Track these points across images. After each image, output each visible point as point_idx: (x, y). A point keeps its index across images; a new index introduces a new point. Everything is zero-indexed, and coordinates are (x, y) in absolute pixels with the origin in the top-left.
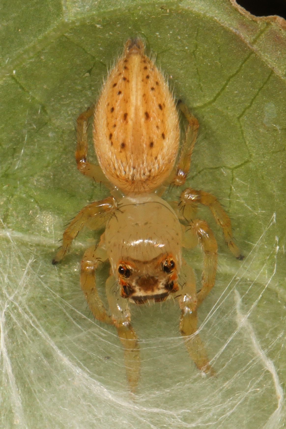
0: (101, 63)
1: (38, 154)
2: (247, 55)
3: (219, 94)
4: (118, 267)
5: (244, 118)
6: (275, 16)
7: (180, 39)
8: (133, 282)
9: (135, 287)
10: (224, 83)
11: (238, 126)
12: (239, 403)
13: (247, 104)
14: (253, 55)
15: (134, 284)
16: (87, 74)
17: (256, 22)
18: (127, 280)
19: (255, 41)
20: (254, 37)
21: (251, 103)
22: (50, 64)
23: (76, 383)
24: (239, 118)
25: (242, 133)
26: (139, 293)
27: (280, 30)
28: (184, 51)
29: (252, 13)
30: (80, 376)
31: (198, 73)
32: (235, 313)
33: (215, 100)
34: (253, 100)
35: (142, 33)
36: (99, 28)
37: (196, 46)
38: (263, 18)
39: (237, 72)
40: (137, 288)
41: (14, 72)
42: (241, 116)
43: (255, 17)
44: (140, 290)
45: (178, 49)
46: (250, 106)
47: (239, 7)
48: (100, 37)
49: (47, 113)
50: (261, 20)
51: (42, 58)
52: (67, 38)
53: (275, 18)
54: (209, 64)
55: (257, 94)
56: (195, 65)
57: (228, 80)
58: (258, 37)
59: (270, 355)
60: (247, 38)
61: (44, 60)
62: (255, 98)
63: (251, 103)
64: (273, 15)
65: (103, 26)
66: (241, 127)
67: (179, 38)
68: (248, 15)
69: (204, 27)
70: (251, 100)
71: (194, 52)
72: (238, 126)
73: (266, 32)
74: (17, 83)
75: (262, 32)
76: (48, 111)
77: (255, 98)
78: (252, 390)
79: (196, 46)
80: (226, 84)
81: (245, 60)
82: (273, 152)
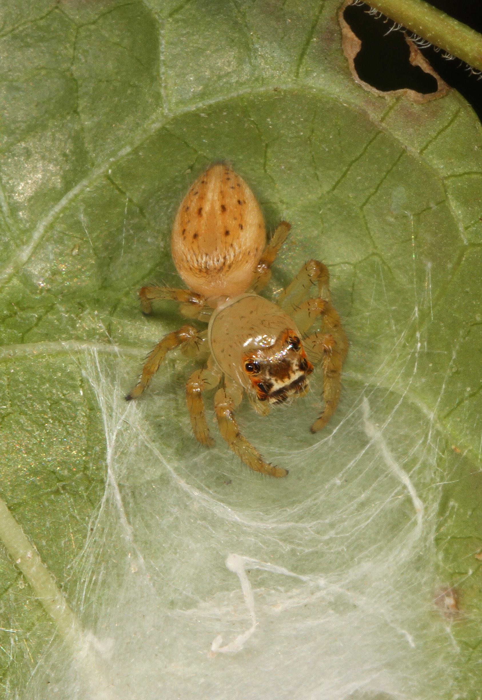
0: (204, 157)
1: (136, 263)
2: (374, 135)
3: (338, 182)
4: (245, 367)
5: (368, 206)
6: (405, 90)
7: (294, 125)
8: (266, 375)
9: (270, 379)
10: (344, 169)
11: (361, 216)
12: (375, 514)
13: (372, 190)
14: (381, 135)
15: (268, 377)
16: (189, 171)
17: (383, 98)
18: (259, 377)
19: (383, 119)
20: (382, 115)
21: (377, 189)
22: (149, 161)
23: (196, 506)
24: (361, 208)
25: (366, 223)
26: (277, 385)
27: (412, 104)
28: (300, 137)
29: (378, 88)
30: (200, 498)
31: (314, 161)
32: (363, 423)
33: (334, 188)
34: (379, 185)
35: (250, 120)
36: (203, 117)
37: (313, 131)
38: (392, 92)
39: (361, 155)
40: (273, 381)
41: (110, 171)
42: (364, 204)
43: (381, 92)
44: (276, 380)
45: (291, 135)
46: (376, 192)
47: (363, 84)
48: (203, 128)
49: (145, 217)
50: (389, 96)
51: (140, 154)
52: (167, 130)
53: (406, 92)
54: (327, 150)
55: (385, 178)
56: (311, 152)
57: (350, 165)
58: (387, 114)
59: (407, 467)
60: (374, 116)
61: (142, 157)
62: (382, 182)
63: (377, 189)
64: (403, 88)
65: (209, 115)
66: (364, 217)
67: (293, 123)
68: (375, 92)
69: (323, 109)
70: (376, 186)
71: (309, 138)
72: (361, 216)
73: (396, 108)
74: (113, 183)
75: (391, 108)
76: (147, 215)
77: (382, 182)
78: (389, 502)
79: (313, 131)
80: (348, 170)
81: (371, 142)
82: (403, 242)
